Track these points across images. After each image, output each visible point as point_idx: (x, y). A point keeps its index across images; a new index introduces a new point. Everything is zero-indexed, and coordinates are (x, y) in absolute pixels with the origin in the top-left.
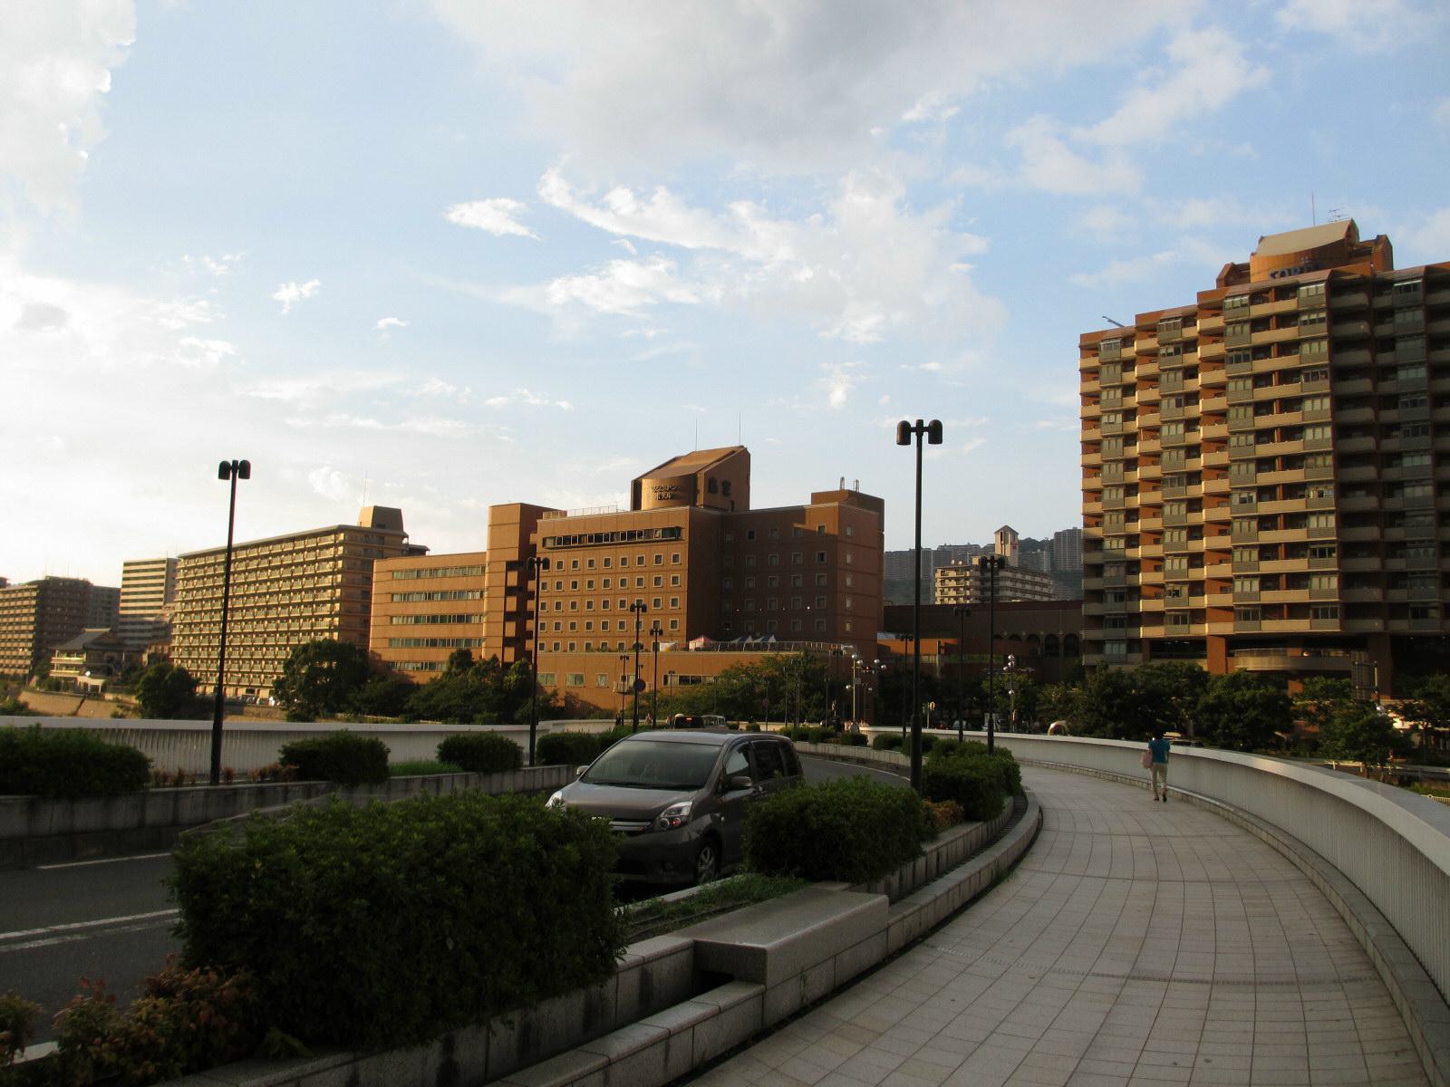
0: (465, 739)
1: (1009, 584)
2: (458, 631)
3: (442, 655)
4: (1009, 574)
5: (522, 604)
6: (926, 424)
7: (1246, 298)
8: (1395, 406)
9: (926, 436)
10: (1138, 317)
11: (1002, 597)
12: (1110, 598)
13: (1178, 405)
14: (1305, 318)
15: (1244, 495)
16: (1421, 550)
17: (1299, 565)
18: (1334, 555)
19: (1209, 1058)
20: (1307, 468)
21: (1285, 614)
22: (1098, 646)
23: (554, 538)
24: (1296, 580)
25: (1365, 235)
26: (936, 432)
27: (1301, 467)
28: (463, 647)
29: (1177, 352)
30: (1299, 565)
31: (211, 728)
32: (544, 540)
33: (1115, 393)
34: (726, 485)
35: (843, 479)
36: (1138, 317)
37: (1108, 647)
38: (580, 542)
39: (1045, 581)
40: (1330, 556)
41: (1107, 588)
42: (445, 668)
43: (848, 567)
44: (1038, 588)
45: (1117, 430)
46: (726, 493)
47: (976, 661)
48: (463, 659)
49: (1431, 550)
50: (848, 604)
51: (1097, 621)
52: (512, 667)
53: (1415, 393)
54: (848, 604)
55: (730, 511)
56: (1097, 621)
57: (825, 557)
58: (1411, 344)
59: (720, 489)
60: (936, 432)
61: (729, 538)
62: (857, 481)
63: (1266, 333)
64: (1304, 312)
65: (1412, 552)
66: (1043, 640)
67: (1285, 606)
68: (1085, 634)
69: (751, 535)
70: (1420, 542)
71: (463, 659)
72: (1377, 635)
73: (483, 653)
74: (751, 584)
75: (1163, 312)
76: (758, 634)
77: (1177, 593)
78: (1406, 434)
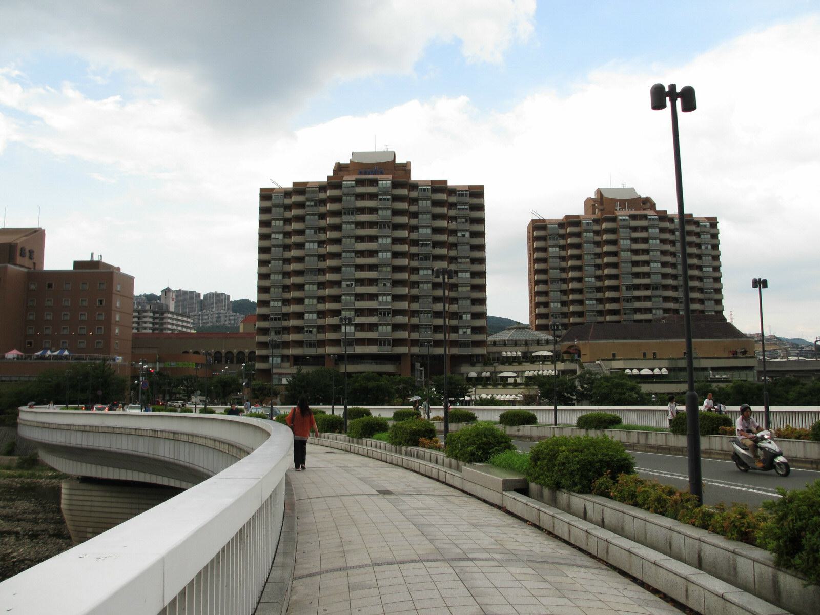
0: (525, 412)
1: (170, 321)
4: (170, 315)
6: (679, 90)
7: (354, 183)
8: (417, 245)
9: (679, 102)
10: (295, 184)
11: (166, 328)
12: (272, 333)
13: (315, 233)
14: (459, 207)
15: (348, 283)
16: (426, 315)
17: (373, 319)
22: (264, 359)
24: (372, 327)
25: (399, 160)
26: (688, 99)
27: (376, 271)
29: (316, 205)
30: (373, 319)
31: (554, 409)
34: (31, 252)
35: (92, 254)
36: (295, 184)
39: (189, 320)
40: (388, 315)
41: (271, 328)
43: (118, 310)
44: (185, 324)
45: (280, 243)
46: (31, 258)
49: (430, 315)
50: (117, 331)
53: (425, 240)
54: (117, 331)
55: (32, 269)
57: (104, 303)
58: (425, 216)
59: (28, 254)
60: (688, 99)
61: (33, 287)
62: (101, 256)
63: (362, 202)
64: (381, 195)
65: (422, 315)
66: (213, 354)
67: (366, 340)
68: (259, 352)
69: (50, 286)
70: (425, 311)
72: (405, 354)
74: (49, 317)
76: (53, 349)
77: (311, 331)
78: (421, 259)
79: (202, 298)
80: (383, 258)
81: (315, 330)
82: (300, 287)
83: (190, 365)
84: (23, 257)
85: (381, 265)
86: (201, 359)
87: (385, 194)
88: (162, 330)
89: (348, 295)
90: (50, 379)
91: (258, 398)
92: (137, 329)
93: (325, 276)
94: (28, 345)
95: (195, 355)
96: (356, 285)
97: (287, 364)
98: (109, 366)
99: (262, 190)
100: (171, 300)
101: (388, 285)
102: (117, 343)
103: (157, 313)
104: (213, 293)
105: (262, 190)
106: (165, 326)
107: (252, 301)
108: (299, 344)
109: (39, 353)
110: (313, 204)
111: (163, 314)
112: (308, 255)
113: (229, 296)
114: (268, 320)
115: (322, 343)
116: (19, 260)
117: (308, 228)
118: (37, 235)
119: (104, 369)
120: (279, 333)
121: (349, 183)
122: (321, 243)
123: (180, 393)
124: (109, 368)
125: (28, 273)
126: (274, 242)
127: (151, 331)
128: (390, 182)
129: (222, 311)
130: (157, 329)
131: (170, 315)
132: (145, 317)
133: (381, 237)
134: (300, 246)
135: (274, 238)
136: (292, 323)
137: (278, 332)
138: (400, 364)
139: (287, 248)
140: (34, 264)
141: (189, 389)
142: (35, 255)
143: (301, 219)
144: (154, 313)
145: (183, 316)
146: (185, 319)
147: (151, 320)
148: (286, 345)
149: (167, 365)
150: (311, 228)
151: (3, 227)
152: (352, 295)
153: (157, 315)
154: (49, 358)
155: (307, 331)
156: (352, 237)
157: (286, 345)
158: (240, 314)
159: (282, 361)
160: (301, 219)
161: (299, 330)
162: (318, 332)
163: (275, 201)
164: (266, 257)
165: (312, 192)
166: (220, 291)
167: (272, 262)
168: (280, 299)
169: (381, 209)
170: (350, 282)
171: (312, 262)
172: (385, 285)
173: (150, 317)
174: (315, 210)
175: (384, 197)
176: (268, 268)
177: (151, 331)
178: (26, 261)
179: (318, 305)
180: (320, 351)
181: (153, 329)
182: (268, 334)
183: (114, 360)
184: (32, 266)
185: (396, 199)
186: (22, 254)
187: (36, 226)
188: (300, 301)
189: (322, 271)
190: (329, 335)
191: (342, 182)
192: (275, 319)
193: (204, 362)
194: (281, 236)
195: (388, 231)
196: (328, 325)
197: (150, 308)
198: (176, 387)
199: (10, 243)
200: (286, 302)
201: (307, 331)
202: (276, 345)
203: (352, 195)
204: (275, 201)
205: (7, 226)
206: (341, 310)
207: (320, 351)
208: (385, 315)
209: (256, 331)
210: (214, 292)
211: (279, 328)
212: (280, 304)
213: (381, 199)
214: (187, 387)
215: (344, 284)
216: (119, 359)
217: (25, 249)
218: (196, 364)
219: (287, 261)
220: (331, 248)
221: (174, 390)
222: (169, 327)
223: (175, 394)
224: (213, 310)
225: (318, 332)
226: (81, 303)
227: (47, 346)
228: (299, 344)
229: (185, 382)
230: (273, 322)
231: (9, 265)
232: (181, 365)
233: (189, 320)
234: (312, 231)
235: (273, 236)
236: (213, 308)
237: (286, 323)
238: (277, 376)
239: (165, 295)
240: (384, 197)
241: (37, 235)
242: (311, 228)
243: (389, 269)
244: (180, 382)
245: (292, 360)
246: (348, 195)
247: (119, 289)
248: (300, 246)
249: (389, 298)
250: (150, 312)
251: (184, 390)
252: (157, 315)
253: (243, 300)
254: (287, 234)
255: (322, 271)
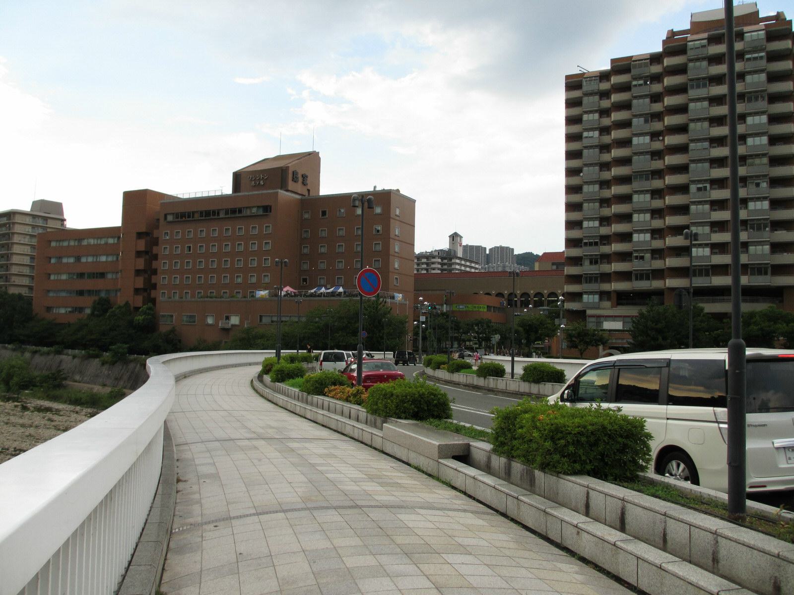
2: (99, 284)
3: (87, 303)
4: (458, 261)
5: (149, 263)
10: (613, 61)
11: (454, 269)
12: (587, 263)
13: (646, 121)
14: (747, 56)
18: (767, 229)
19: (215, 528)
20: (749, 166)
21: (697, 274)
22: (576, 296)
23: (173, 214)
28: (103, 295)
32: (166, 216)
33: (94, 242)
34: (304, 177)
36: (613, 61)
37: (585, 296)
38: (193, 217)
39: (477, 266)
40: (765, 228)
42: (88, 311)
45: (596, 142)
46: (304, 184)
47: (470, 309)
48: (103, 306)
51: (575, 279)
52: (140, 310)
56: (575, 279)
59: (300, 179)
61: (306, 216)
64: (749, 52)
66: (506, 297)
69: (324, 213)
71: (103, 306)
73: (120, 300)
74: (323, 250)
75: (632, 57)
76: (328, 286)
77: (642, 258)
79: (488, 252)
80: (754, 146)
81: (648, 256)
82: (626, 199)
83: (481, 308)
84: (295, 182)
85: (751, 156)
86: (495, 301)
87: (756, 50)
88: (451, 270)
89: (700, 203)
90: (317, 319)
91: (576, 347)
92: (427, 270)
93: (609, 227)
94: (304, 282)
95: (486, 296)
96: (711, 188)
97: (607, 304)
98: (383, 304)
99: (567, 77)
100: (459, 245)
101: (764, 185)
102: (396, 278)
103: (445, 259)
104: (498, 247)
105: (567, 77)
106: (453, 267)
107: (535, 254)
108: (625, 276)
109: (313, 291)
110: (641, 82)
111: (451, 260)
112: (635, 154)
113: (513, 249)
114: (581, 246)
115: (659, 274)
116: (291, 185)
117: (635, 116)
118: (312, 159)
119: (377, 307)
120: (596, 263)
121: (696, 42)
122: (655, 135)
123: (470, 340)
124: (384, 306)
125: (301, 200)
126: (586, 142)
127: (439, 272)
128: (763, 32)
129: (507, 263)
130: (445, 270)
131: (458, 261)
132: (433, 263)
133: (750, 114)
134: (625, 143)
135: (587, 137)
136: (616, 247)
137: (594, 261)
138: (782, 301)
139: (605, 148)
140: (309, 190)
141: (481, 336)
142: (309, 181)
143: (625, 106)
144: (442, 259)
145: (471, 262)
146: (473, 265)
147: (439, 266)
148: (606, 277)
149: (454, 308)
150: (640, 116)
151: (278, 154)
152: (705, 202)
153: (446, 261)
154: (321, 295)
155: (636, 257)
156: (704, 119)
157: (606, 277)
158: (524, 266)
159: (601, 299)
160: (625, 106)
161: (624, 256)
162: (653, 258)
163: (586, 87)
164: (576, 163)
165: (640, 66)
166: (504, 245)
167: (585, 169)
168: (597, 218)
169: (750, 73)
170: (703, 184)
171: (642, 163)
172: (758, 185)
173: (439, 263)
174: (645, 91)
175: (756, 55)
176: (579, 177)
177: (439, 272)
178: (298, 187)
179: (653, 221)
180: (656, 284)
181: (442, 270)
182: (581, 265)
183: (393, 298)
184: (306, 193)
185: (773, 57)
186: (295, 179)
187: (310, 150)
188: (626, 218)
189: (658, 174)
190: (672, 262)
191: (686, 45)
192: (591, 244)
193: (497, 305)
194: (596, 133)
195: (762, 105)
196: (614, 272)
197: (439, 254)
198: (466, 333)
199: (282, 167)
200: (605, 221)
201: (636, 257)
202: (590, 278)
203: (704, 59)
204: (586, 87)
205: (282, 153)
206: (689, 225)
207: (656, 284)
208: (759, 229)
209: (563, 261)
210: (499, 246)
211: (596, 255)
212: (597, 223)
213: (749, 59)
214: (477, 333)
215: (693, 188)
216: (399, 297)
217: (297, 173)
218: (488, 306)
219: (605, 166)
220: (671, 140)
221: (464, 337)
222: (458, 267)
223: (464, 341)
224: (499, 263)
225: (653, 258)
226: (375, 248)
227: (322, 282)
228: (625, 276)
229: (476, 328)
230: (588, 248)
231: (279, 191)
232: (470, 307)
233: (477, 266)
234: (642, 120)
235: (585, 134)
236: (498, 261)
237: (605, 249)
238: (593, 319)
239: (453, 240)
240: (756, 55)
241: (312, 159)
242: (640, 116)
243: (765, 160)
244: (470, 327)
245: (614, 296)
246: (698, 60)
247: (398, 213)
248: (625, 143)
249: (766, 205)
250: (438, 258)
251: (475, 337)
252: (446, 261)
253: (526, 253)
254: (605, 130)
255: (658, 174)
